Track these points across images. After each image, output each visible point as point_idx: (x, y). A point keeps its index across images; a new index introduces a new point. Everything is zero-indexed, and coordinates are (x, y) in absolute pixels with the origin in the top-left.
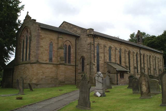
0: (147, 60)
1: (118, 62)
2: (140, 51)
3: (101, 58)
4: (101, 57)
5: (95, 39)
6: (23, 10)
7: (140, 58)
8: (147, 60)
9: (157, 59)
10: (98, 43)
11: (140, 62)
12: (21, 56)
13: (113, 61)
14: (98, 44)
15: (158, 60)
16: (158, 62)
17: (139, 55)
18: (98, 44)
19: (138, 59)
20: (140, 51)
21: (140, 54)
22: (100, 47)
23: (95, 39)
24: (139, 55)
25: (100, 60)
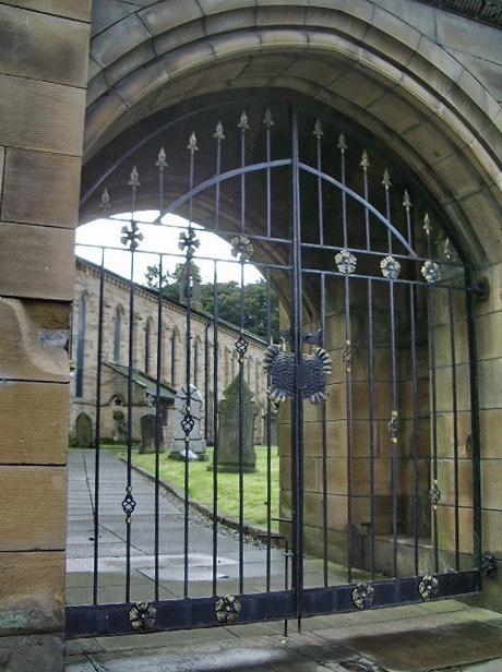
0: (227, 367)
1: (153, 373)
2: (206, 330)
3: (92, 347)
4: (91, 341)
5: (213, 282)
6: (107, 670)
7: (206, 359)
8: (227, 367)
9: (254, 365)
10: (83, 288)
11: (204, 372)
12: (164, 77)
13: (140, 366)
14: (85, 293)
15: (257, 368)
16: (257, 378)
17: (204, 344)
18: (85, 293)
19: (199, 361)
20: (206, 330)
21: (188, 334)
22: (87, 305)
23: (213, 282)
24: (204, 348)
25: (87, 355)
